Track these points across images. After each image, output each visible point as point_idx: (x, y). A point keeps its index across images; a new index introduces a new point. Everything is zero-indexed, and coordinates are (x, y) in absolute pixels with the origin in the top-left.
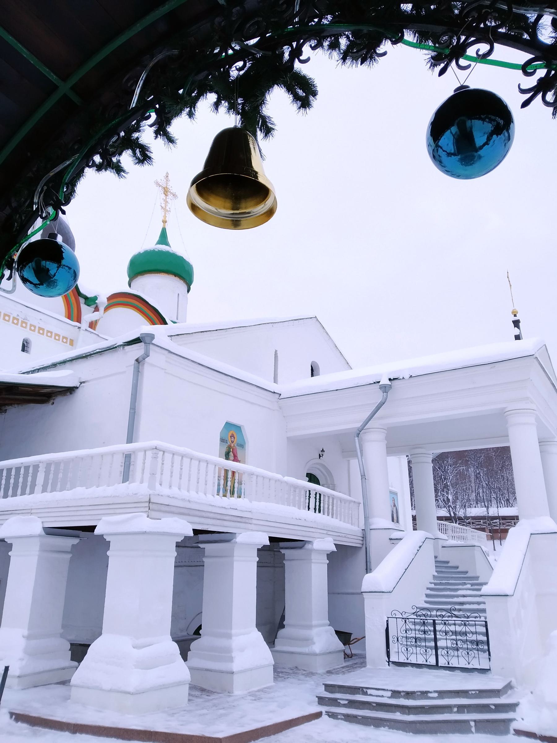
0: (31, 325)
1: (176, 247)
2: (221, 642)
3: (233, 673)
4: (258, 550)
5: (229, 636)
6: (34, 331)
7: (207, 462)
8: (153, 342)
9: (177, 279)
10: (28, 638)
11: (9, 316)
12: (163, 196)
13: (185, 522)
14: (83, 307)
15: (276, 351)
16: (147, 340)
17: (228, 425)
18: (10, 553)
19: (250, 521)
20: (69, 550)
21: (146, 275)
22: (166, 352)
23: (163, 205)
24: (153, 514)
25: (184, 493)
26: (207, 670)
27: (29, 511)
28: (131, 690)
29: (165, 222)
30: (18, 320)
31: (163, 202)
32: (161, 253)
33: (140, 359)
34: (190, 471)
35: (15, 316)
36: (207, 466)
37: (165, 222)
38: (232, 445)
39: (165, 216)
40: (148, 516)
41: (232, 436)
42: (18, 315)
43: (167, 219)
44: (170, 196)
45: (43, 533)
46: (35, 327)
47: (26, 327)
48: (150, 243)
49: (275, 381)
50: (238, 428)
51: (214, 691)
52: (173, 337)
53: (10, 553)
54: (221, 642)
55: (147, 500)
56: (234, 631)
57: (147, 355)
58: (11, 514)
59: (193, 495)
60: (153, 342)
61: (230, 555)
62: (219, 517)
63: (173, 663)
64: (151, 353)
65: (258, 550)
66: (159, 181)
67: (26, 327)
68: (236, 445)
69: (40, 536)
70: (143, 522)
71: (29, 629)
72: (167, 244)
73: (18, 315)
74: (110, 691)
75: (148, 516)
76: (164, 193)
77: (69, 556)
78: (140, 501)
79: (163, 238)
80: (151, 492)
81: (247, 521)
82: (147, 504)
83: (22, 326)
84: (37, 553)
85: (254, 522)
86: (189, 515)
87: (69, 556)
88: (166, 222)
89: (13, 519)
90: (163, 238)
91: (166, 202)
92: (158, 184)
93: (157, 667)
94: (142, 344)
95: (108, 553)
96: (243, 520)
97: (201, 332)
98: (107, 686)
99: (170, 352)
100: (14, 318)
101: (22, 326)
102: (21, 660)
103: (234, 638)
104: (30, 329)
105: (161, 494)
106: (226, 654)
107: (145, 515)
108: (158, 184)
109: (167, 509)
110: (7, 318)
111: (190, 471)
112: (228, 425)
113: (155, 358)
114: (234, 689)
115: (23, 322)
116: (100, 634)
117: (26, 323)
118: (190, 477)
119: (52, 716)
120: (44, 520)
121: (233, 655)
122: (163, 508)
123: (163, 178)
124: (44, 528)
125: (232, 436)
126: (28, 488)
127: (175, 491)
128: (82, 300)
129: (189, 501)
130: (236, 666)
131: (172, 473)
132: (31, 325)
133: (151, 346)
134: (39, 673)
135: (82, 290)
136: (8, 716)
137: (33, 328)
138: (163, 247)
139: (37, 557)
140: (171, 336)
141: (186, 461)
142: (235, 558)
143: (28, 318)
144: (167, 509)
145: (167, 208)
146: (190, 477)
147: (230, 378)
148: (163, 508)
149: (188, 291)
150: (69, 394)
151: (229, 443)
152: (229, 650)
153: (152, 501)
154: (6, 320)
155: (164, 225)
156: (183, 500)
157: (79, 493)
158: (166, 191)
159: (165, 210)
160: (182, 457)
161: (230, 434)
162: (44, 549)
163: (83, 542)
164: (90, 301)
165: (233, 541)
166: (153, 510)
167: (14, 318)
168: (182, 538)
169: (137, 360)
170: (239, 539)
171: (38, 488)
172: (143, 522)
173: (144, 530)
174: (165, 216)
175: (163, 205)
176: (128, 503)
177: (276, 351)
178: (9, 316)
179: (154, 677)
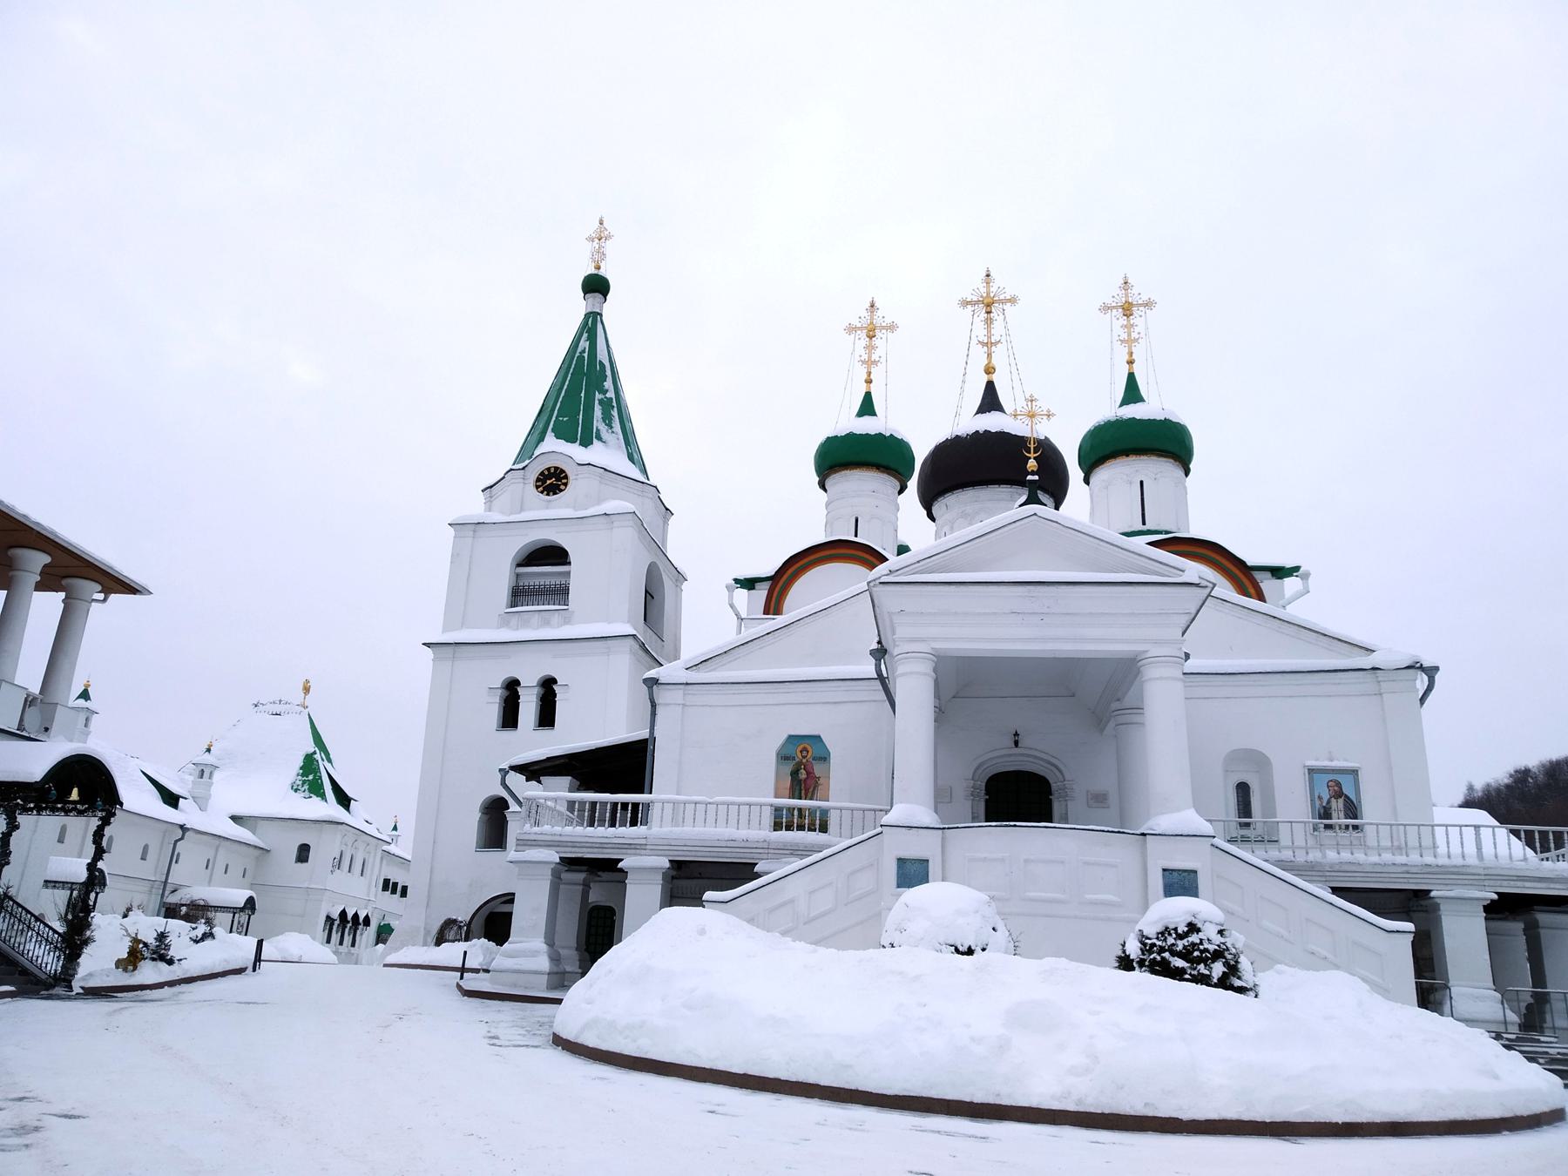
37: (1131, 362)
48: (1107, 407)
65: (1487, 909)
159: (1129, 342)
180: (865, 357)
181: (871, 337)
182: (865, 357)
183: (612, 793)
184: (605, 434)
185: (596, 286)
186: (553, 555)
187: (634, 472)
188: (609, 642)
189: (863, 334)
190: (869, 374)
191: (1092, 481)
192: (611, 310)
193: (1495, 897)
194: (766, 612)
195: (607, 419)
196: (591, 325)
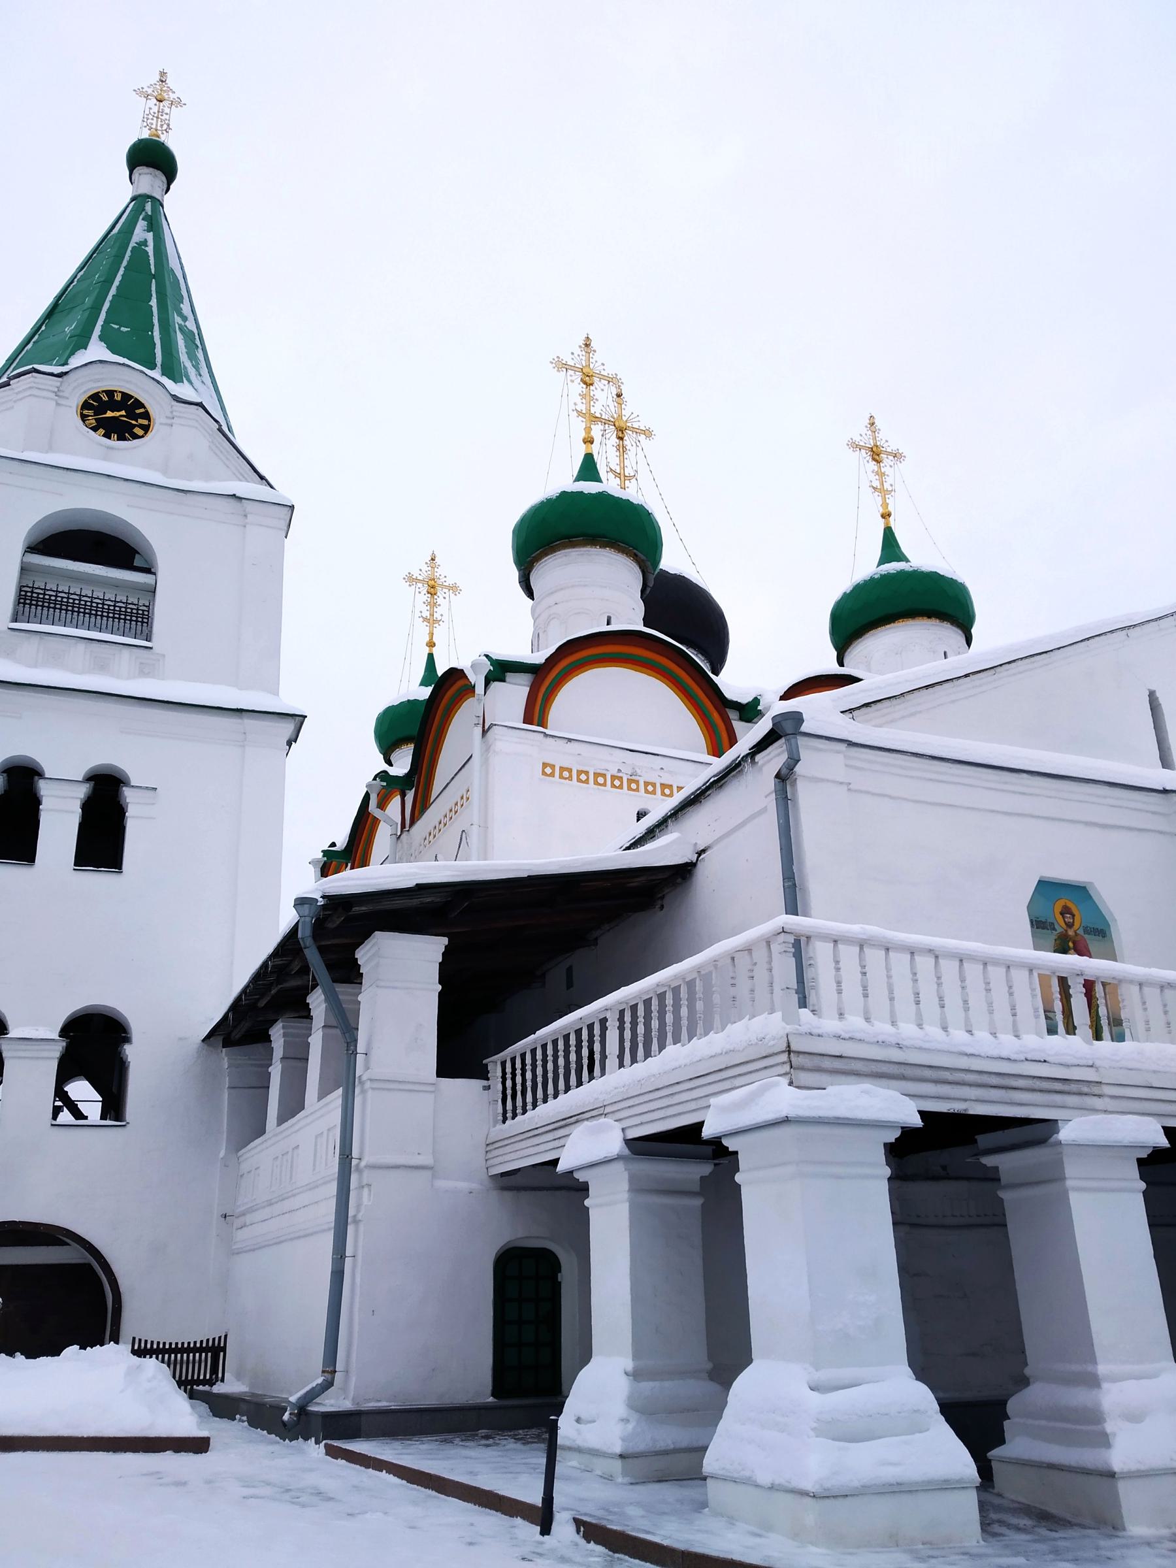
0: (646, 784)
1: (921, 556)
2: (1079, 1397)
3: (1111, 1475)
4: (1141, 1162)
5: (1093, 1382)
6: (654, 792)
7: (935, 955)
8: (804, 728)
9: (934, 622)
10: (636, 1375)
11: (604, 776)
12: (873, 465)
13: (897, 1094)
14: (738, 726)
15: (1152, 695)
16: (788, 727)
17: (1046, 887)
18: (587, 1203)
19: (1096, 1090)
20: (697, 1188)
21: (867, 635)
22: (843, 747)
23: (876, 484)
24: (804, 1077)
25: (882, 1028)
26: (1052, 1466)
27: (601, 1111)
28: (808, 1486)
29: (886, 516)
30: (620, 779)
31: (874, 478)
32: (886, 578)
33: (784, 771)
34: (889, 977)
35: (615, 773)
36: (937, 963)
37: (886, 516)
38: (1071, 933)
39: (885, 504)
40: (791, 1084)
41: (1066, 911)
42: (619, 771)
43: (890, 508)
44: (887, 461)
45: (627, 1152)
46: (654, 785)
47: (637, 790)
48: (866, 564)
49: (1166, 762)
50: (1080, 891)
51: (1074, 1520)
52: (855, 713)
53: (587, 1203)
54: (1079, 1397)
55: (784, 1047)
56: (1102, 1369)
57: (794, 760)
58: (577, 1122)
59: (908, 1030)
60: (804, 728)
61: (1054, 1176)
62: (995, 1081)
63: (920, 1432)
64: (804, 754)
65: (1141, 1162)
66: (857, 439)
67: (637, 790)
68: (1081, 932)
69: (619, 1158)
70: (781, 1097)
71: (636, 1356)
72: (902, 558)
73: (619, 771)
74: (772, 1488)
75: (791, 1084)
76: (874, 459)
77: (698, 1202)
78: (771, 1051)
79: (890, 548)
80: (789, 1028)
81: (1085, 1089)
82: (784, 1057)
83: (630, 789)
84: (626, 1196)
85: (1107, 1090)
86: (903, 1078)
87: (698, 1202)
88: (889, 515)
89: (578, 1132)
90: (890, 548)
91: (881, 475)
92: (855, 446)
93: (880, 1438)
94: (782, 741)
95: (738, 1178)
96: (1073, 1087)
97: (927, 687)
98: (764, 1478)
99: (851, 744)
100: (613, 777)
101: (630, 789)
102: (625, 1421)
103: (1105, 1385)
104: (647, 791)
105: (815, 1031)
106: (1089, 1426)
107: (784, 1081)
108: (855, 446)
109: (838, 1064)
110: (601, 780)
111: (889, 977)
112: (1046, 887)
113: (812, 761)
114: (1125, 1519)
115: (630, 781)
116: (749, 1361)
117: (637, 782)
118: (891, 991)
119: (648, 1532)
120: (625, 1124)
121: (1109, 1427)
122: (827, 1063)
123: (864, 431)
124: (629, 1142)
125: (1066, 911)
126: (591, 1066)
127: (855, 1023)
128: (733, 715)
129: (899, 1046)
130: (1119, 1458)
131: (839, 983)
132: (646, 784)
133: (802, 741)
134: (666, 1453)
135: (729, 694)
136: (573, 1528)
137: (650, 788)
138: (893, 567)
139: (627, 1205)
140: (851, 710)
141: (874, 957)
142: (1069, 1183)
143: (639, 772)
144: (838, 1064)
145: (887, 486)
146: (891, 991)
147: (1025, 775)
148: (827, 1063)
149: (969, 641)
150: (679, 880)
151: (1059, 930)
152: (1094, 1417)
153: (793, 1048)
154: (582, 782)
155: (887, 523)
156: (882, 1044)
157: (674, 1058)
158: (876, 454)
159: (882, 492)
160: (861, 947)
161: (1058, 908)
162: (638, 1187)
163: (693, 1163)
164: (750, 711)
165: (1052, 1140)
166: (802, 1068)
167: (613, 777)
168: (898, 1134)
169: (778, 776)
170: (1065, 1134)
171: (612, 1061)
172: (781, 1097)
173: (784, 1114)
174: (885, 504)
175: (876, 484)
176: (747, 1062)
177: (1152, 695)
178: (604, 776)
179: (866, 1462)
180: (426, 614)
181: (588, 385)
182: (426, 614)
183: (1145, 966)
184: (192, 372)
185: (152, 157)
186: (111, 547)
187: (249, 488)
188: (249, 723)
189: (424, 589)
190: (431, 634)
191: (846, 662)
192: (178, 205)
193: (917, 1122)
194: (528, 719)
195: (192, 357)
196: (146, 210)
